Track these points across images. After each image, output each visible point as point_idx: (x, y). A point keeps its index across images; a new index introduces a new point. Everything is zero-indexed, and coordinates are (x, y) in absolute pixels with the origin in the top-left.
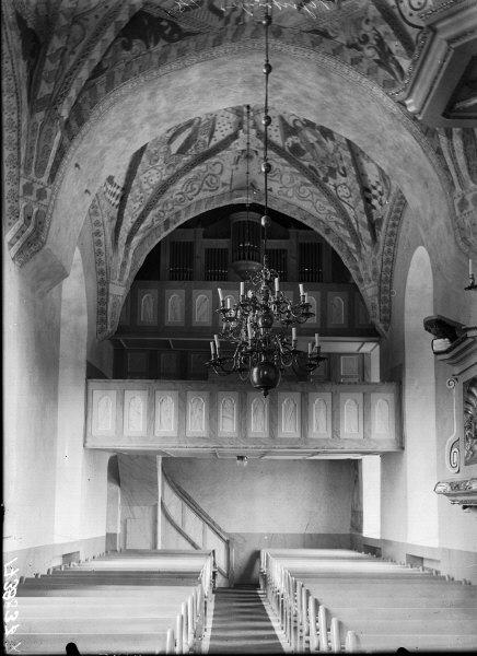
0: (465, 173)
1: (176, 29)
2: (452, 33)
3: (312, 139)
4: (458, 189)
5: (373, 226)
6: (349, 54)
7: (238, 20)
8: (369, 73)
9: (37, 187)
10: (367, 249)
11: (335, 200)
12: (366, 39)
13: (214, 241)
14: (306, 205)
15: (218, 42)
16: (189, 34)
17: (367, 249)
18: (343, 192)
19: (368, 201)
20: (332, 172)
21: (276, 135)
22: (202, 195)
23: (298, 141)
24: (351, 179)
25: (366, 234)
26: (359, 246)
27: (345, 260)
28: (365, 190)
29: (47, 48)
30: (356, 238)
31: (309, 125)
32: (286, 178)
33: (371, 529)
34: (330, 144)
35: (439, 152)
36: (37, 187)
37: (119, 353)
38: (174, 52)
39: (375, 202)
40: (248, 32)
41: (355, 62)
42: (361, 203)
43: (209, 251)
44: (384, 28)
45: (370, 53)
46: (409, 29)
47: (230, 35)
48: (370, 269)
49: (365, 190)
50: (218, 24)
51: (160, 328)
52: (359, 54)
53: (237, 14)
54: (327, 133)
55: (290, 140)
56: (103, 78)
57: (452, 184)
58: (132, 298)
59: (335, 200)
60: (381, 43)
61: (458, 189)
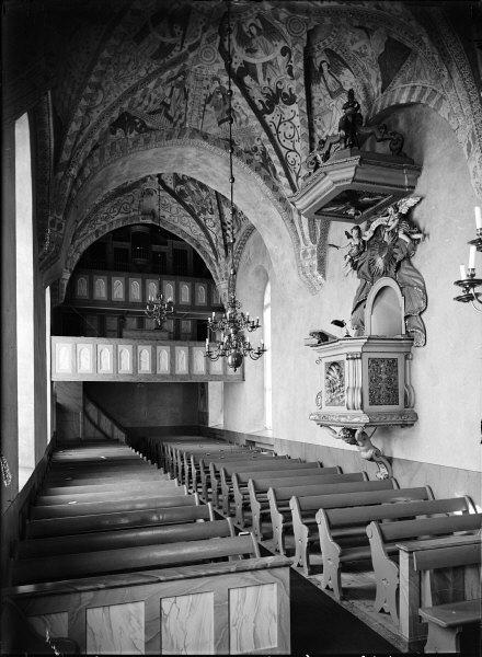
0: (307, 237)
1: (144, 125)
2: (337, 178)
3: (193, 188)
4: (302, 244)
5: (226, 246)
6: (246, 156)
7: (181, 125)
8: (257, 170)
9: (57, 221)
10: (222, 260)
11: (204, 228)
12: (256, 149)
13: (120, 243)
14: (186, 229)
15: (170, 137)
16: (152, 129)
17: (222, 260)
18: (209, 223)
19: (224, 231)
20: (204, 211)
21: (170, 184)
22: (119, 216)
23: (183, 188)
24: (215, 217)
25: (222, 251)
26: (216, 257)
27: (208, 265)
28: (223, 224)
29: (67, 129)
30: (215, 252)
31: (192, 180)
32: (174, 210)
33: (215, 420)
34: (204, 194)
35: (292, 221)
36: (57, 221)
37: (203, 387)
38: (142, 140)
39: (228, 232)
40: (188, 134)
41: (249, 162)
42: (221, 232)
43: (117, 250)
44: (269, 146)
45: (257, 158)
46: (282, 149)
47: (177, 133)
48: (224, 272)
49: (223, 224)
50: (169, 126)
51: (110, 302)
52: (250, 157)
53: (181, 121)
54: (203, 187)
55: (179, 187)
56: (98, 151)
57: (299, 241)
58: (72, 282)
59: (204, 228)
60: (264, 153)
61: (302, 244)
